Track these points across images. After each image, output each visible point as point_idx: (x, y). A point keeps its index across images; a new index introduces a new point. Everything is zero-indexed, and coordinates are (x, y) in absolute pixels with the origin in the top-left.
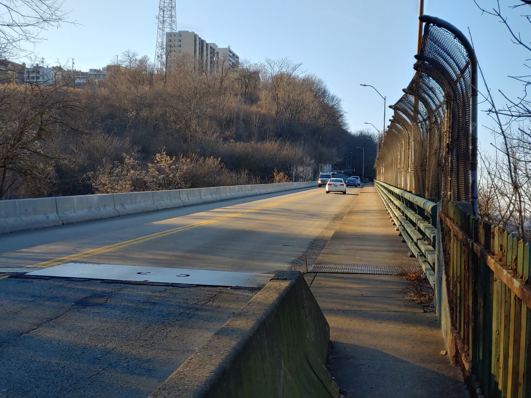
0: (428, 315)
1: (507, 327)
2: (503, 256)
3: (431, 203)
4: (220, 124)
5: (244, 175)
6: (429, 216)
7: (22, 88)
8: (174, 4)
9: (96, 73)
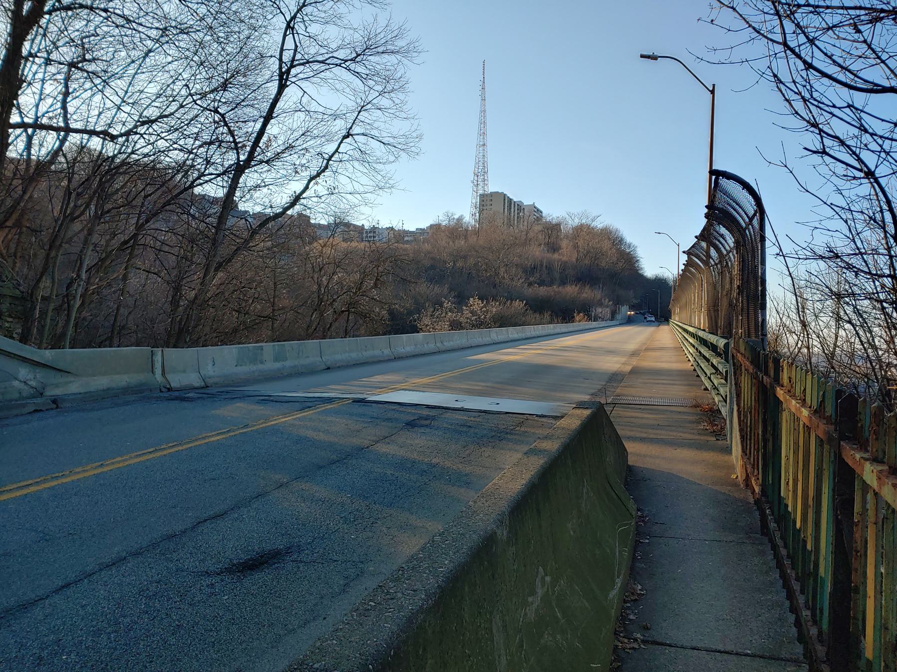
0: (720, 442)
1: (796, 452)
2: (792, 387)
3: (723, 340)
4: (525, 271)
5: (547, 316)
6: (722, 352)
7: (362, 245)
8: (486, 169)
9: (421, 231)
